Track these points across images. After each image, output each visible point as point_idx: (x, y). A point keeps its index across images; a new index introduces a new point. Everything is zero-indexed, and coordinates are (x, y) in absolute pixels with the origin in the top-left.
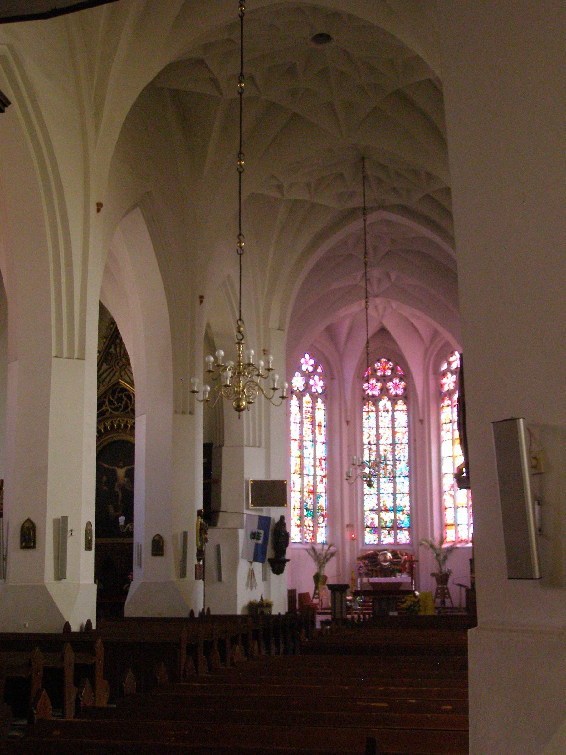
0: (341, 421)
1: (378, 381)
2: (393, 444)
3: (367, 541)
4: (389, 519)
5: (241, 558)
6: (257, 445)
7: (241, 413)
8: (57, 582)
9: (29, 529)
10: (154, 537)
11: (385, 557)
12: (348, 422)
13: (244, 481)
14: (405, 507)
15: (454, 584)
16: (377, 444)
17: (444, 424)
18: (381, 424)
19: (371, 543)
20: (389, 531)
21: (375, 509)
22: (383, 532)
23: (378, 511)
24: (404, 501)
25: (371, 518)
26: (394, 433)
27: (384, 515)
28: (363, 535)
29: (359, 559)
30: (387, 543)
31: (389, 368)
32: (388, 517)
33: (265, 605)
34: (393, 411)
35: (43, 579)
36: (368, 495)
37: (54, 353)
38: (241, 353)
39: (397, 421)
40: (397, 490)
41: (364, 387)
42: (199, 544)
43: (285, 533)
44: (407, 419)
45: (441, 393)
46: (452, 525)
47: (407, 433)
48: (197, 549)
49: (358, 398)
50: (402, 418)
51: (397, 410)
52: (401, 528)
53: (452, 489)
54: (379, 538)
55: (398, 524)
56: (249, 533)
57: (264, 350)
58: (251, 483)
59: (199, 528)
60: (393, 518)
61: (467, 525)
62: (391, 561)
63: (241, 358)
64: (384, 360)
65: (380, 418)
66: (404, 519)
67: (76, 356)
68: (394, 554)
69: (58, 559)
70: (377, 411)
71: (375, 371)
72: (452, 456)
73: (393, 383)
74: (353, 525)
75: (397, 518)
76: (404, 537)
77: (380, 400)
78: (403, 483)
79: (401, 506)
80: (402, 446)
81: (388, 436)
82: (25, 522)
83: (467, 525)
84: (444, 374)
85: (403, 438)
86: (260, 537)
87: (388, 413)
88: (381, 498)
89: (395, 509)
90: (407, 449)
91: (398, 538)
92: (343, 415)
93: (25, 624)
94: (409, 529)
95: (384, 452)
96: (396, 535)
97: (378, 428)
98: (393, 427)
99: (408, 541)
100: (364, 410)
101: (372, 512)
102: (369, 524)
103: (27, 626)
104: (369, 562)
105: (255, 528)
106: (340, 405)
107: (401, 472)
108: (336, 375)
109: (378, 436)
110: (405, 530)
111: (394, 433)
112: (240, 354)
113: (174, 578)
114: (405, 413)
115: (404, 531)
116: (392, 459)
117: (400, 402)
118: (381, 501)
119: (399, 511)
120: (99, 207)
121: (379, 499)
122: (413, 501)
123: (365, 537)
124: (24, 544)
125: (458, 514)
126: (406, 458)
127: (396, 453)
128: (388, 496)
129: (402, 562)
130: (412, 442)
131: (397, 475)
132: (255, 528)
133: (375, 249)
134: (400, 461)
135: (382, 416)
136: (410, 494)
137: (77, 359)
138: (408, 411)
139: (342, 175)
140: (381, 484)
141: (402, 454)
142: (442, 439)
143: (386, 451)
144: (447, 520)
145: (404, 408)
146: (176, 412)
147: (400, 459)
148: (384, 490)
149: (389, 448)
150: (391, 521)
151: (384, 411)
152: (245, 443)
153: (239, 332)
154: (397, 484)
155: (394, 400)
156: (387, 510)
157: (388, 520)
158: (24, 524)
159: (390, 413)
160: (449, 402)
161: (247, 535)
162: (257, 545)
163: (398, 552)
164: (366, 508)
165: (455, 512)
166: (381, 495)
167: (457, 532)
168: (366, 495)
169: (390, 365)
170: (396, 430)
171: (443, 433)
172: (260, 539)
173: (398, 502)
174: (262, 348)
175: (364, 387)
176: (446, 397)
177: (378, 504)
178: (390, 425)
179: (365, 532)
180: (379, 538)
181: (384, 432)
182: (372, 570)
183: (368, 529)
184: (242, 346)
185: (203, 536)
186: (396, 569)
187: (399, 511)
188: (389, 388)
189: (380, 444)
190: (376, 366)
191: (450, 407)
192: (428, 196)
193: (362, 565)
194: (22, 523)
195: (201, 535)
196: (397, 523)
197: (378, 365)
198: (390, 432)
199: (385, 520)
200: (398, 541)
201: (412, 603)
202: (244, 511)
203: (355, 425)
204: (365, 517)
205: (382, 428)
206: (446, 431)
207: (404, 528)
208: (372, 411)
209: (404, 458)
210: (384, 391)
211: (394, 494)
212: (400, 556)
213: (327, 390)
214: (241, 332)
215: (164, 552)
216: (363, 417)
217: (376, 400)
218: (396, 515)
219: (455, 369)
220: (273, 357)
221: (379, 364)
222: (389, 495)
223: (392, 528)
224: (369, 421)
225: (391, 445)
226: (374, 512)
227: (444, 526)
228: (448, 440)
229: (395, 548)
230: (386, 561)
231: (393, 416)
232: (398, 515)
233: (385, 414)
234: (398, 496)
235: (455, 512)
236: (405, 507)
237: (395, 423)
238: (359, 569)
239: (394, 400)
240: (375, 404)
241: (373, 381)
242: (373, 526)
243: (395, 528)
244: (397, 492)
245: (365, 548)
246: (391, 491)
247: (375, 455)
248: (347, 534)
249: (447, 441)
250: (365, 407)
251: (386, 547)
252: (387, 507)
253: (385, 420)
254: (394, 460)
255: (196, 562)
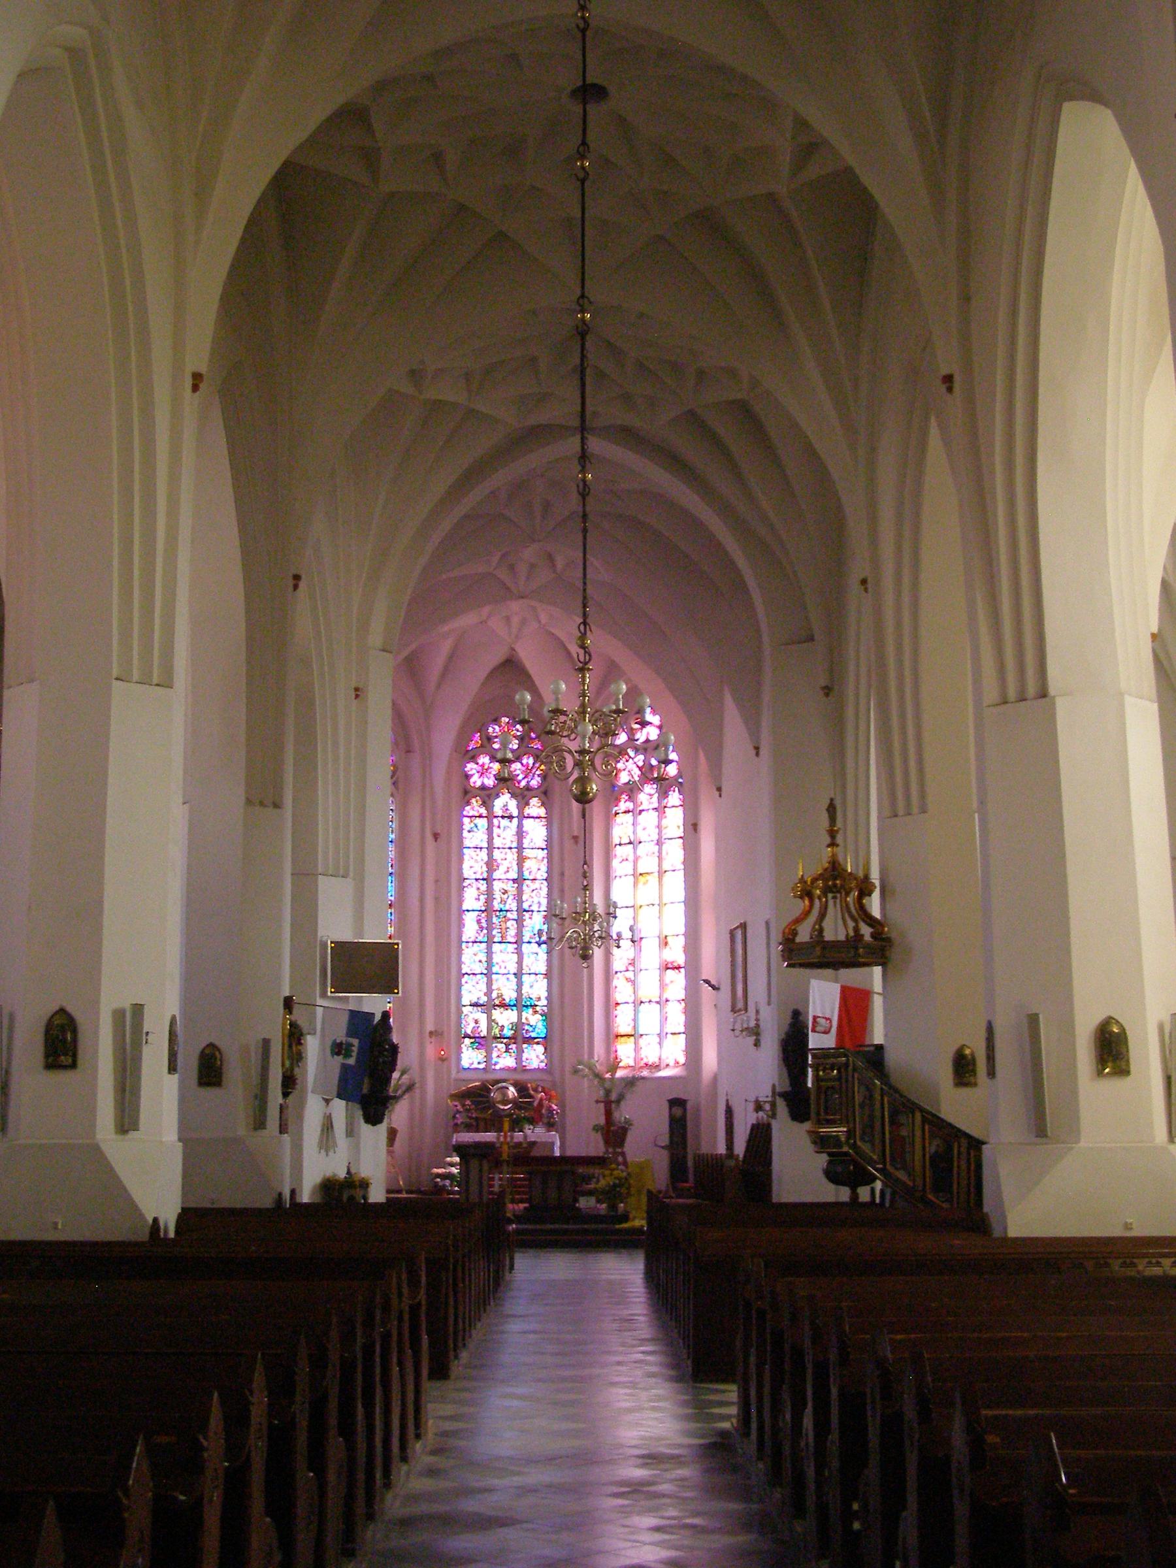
0: (423, 831)
1: (493, 759)
2: (519, 881)
3: (465, 1063)
4: (508, 1022)
5: (312, 1092)
6: (341, 872)
7: (587, 806)
8: (120, 1137)
9: (62, 1029)
10: (204, 1049)
11: (505, 1095)
12: (436, 836)
13: (318, 943)
14: (539, 999)
15: (656, 1145)
16: (489, 880)
17: (618, 846)
18: (497, 842)
19: (473, 1067)
20: (507, 1045)
21: (481, 1002)
22: (496, 1047)
23: (488, 1007)
24: (537, 989)
25: (475, 1020)
26: (521, 860)
27: (497, 1014)
28: (459, 1051)
29: (454, 1097)
30: (502, 1067)
31: (515, 737)
32: (506, 1018)
33: (357, 1184)
34: (522, 817)
35: (94, 1133)
36: (469, 975)
37: (115, 672)
38: (586, 688)
39: (528, 837)
40: (524, 967)
41: (466, 769)
42: (287, 1063)
43: (389, 1045)
44: (546, 834)
45: (614, 786)
46: (629, 1036)
47: (546, 860)
48: (283, 1074)
49: (456, 792)
50: (536, 832)
51: (529, 817)
52: (530, 1040)
53: (631, 968)
54: (488, 1057)
55: (524, 1031)
56: (329, 1043)
57: (357, 689)
58: (332, 947)
59: (287, 1032)
60: (515, 1019)
61: (659, 1035)
62: (514, 1102)
63: (587, 698)
64: (507, 720)
65: (496, 830)
66: (535, 1023)
67: (136, 677)
68: (522, 1088)
69: (123, 1090)
70: (490, 817)
71: (490, 739)
72: (633, 906)
73: (522, 764)
74: (443, 1032)
75: (524, 1020)
76: (535, 1056)
77: (497, 796)
78: (537, 954)
79: (531, 999)
80: (537, 885)
81: (510, 866)
82: (56, 1013)
83: (659, 1035)
84: (622, 751)
85: (539, 869)
86: (353, 1051)
87: (511, 821)
88: (494, 982)
89: (519, 1004)
90: (545, 891)
91: (524, 1059)
92: (428, 823)
93: (56, 1224)
94: (546, 1041)
95: (503, 896)
96: (520, 1052)
97: (490, 848)
98: (520, 848)
99: (543, 1065)
100: (465, 813)
101: (475, 1008)
102: (469, 1032)
103: (60, 1227)
104: (473, 1102)
105: (341, 1035)
106: (423, 799)
107: (532, 934)
108: (416, 744)
109: (491, 865)
110: (538, 1043)
111: (521, 860)
112: (584, 690)
113: (242, 1130)
114: (544, 822)
115: (535, 1046)
116: (515, 909)
117: (534, 801)
118: (494, 987)
119: (527, 1006)
120: (198, 382)
121: (489, 984)
122: (555, 990)
123: (462, 1055)
124: (50, 1060)
125: (641, 1016)
126: (544, 908)
127: (524, 898)
128: (508, 979)
129: (535, 1104)
130: (556, 878)
131: (526, 939)
132: (341, 1035)
133: (547, 505)
134: (530, 913)
135: (499, 827)
136: (548, 975)
137: (158, 685)
138: (549, 819)
139: (533, 360)
140: (494, 956)
141: (536, 900)
142: (613, 875)
143: (505, 892)
144: (618, 1026)
145: (542, 812)
146: (249, 802)
147: (532, 908)
148: (500, 967)
149: (511, 888)
150: (510, 1026)
151: (503, 817)
152: (320, 870)
153: (583, 646)
154: (525, 956)
155: (524, 797)
156: (504, 1005)
157: (506, 1024)
158: (52, 1016)
159: (515, 821)
160: (630, 805)
161: (324, 1050)
162: (344, 1067)
163: (529, 1085)
164: (465, 1000)
165: (636, 1012)
166: (494, 976)
167: (637, 1049)
168: (466, 976)
169: (518, 731)
170: (526, 853)
171: (615, 863)
172: (351, 1056)
173: (525, 990)
174: (354, 685)
175: (466, 769)
176: (623, 796)
177: (488, 993)
178: (515, 845)
179: (463, 1046)
180: (488, 1057)
181: (503, 856)
182: (477, 1119)
183: (467, 1041)
184: (588, 675)
185: (294, 1048)
186: (524, 1118)
187: (527, 1006)
188: (470, 773)
189: (494, 880)
190: (490, 730)
191: (631, 814)
192: (692, 413)
193: (459, 1108)
194: (50, 1014)
195: (290, 1046)
196: (524, 1029)
197: (494, 729)
198: (512, 856)
199: (500, 1025)
200: (524, 1064)
201: (617, 1181)
202: (315, 1000)
203: (449, 842)
204: (463, 1017)
205: (499, 848)
206: (620, 860)
207: (536, 1040)
208: (480, 816)
209: (539, 907)
210: (505, 781)
211: (518, 975)
212: (532, 1092)
213: (398, 773)
214: (587, 647)
215: (224, 1079)
216: (464, 827)
217: (489, 796)
218: (521, 1015)
219: (644, 742)
220: (650, 700)
221: (497, 728)
222: (508, 976)
223: (513, 1039)
224: (474, 836)
225: (514, 883)
226: (479, 1009)
227: (613, 1037)
228: (626, 875)
229: (517, 1077)
230: (505, 1102)
231: (520, 826)
232: (524, 1015)
233: (505, 822)
234: (525, 978)
235: (636, 1012)
236: (539, 999)
237: (524, 841)
238: (454, 1117)
239: (523, 796)
240: (487, 803)
241: (484, 760)
242: (477, 1035)
243: (520, 1039)
244: (524, 972)
245: (464, 1075)
246: (513, 968)
247: (484, 901)
248: (430, 1051)
249: (623, 878)
250: (467, 808)
251: (504, 1075)
252: (504, 1000)
253: (506, 834)
254: (521, 911)
255: (280, 1100)
